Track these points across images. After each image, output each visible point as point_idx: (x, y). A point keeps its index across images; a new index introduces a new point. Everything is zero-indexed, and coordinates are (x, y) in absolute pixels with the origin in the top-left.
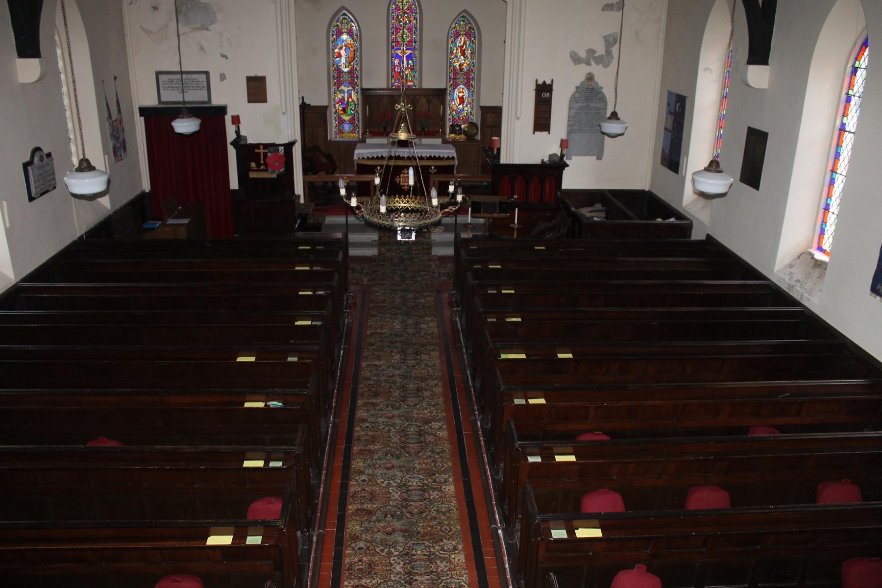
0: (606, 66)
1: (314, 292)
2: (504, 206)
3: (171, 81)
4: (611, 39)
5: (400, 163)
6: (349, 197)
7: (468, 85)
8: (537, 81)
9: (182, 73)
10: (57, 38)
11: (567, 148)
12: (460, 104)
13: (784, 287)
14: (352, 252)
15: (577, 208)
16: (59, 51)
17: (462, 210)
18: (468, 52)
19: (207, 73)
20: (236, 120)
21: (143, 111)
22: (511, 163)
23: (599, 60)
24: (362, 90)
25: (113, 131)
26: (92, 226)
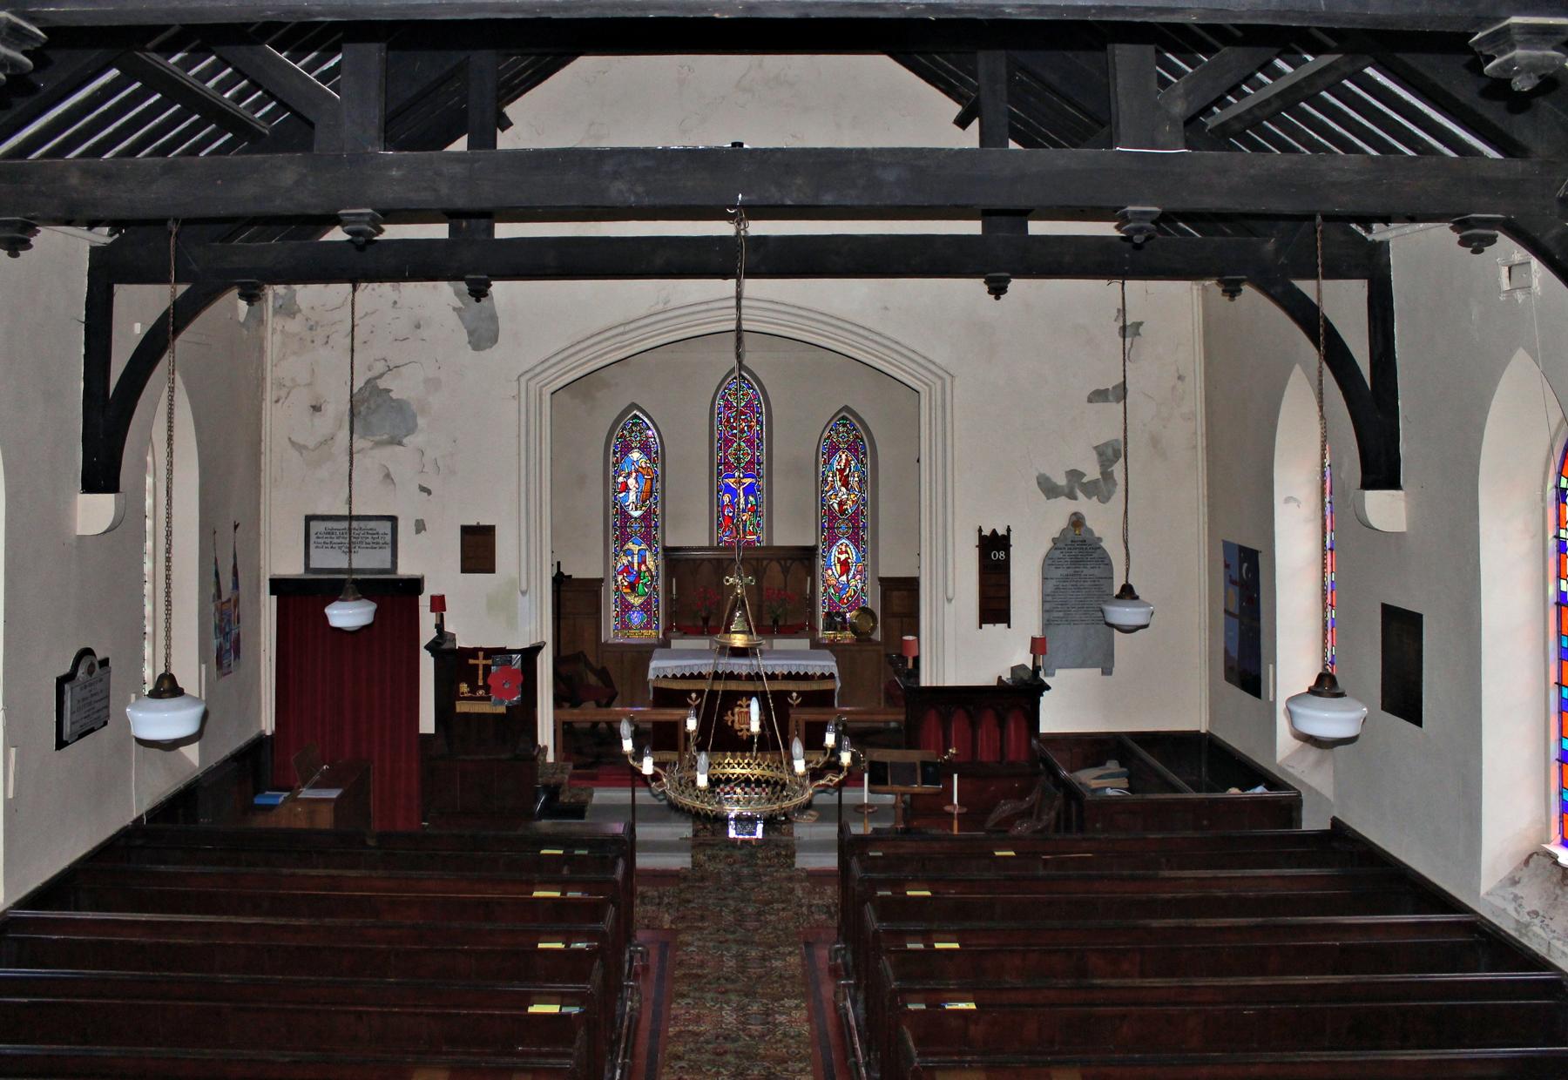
0: (1104, 499)
1: (568, 945)
2: (931, 769)
3: (330, 533)
4: (1110, 452)
5: (733, 686)
6: (639, 755)
7: (855, 539)
8: (980, 530)
9: (351, 518)
10: (149, 459)
11: (1044, 653)
12: (842, 575)
13: (1508, 927)
14: (644, 861)
15: (1071, 771)
16: (149, 480)
17: (853, 778)
18: (853, 481)
19: (393, 520)
20: (438, 604)
21: (278, 585)
22: (940, 684)
23: (1091, 489)
24: (665, 549)
25: (221, 620)
26: (162, 798)
